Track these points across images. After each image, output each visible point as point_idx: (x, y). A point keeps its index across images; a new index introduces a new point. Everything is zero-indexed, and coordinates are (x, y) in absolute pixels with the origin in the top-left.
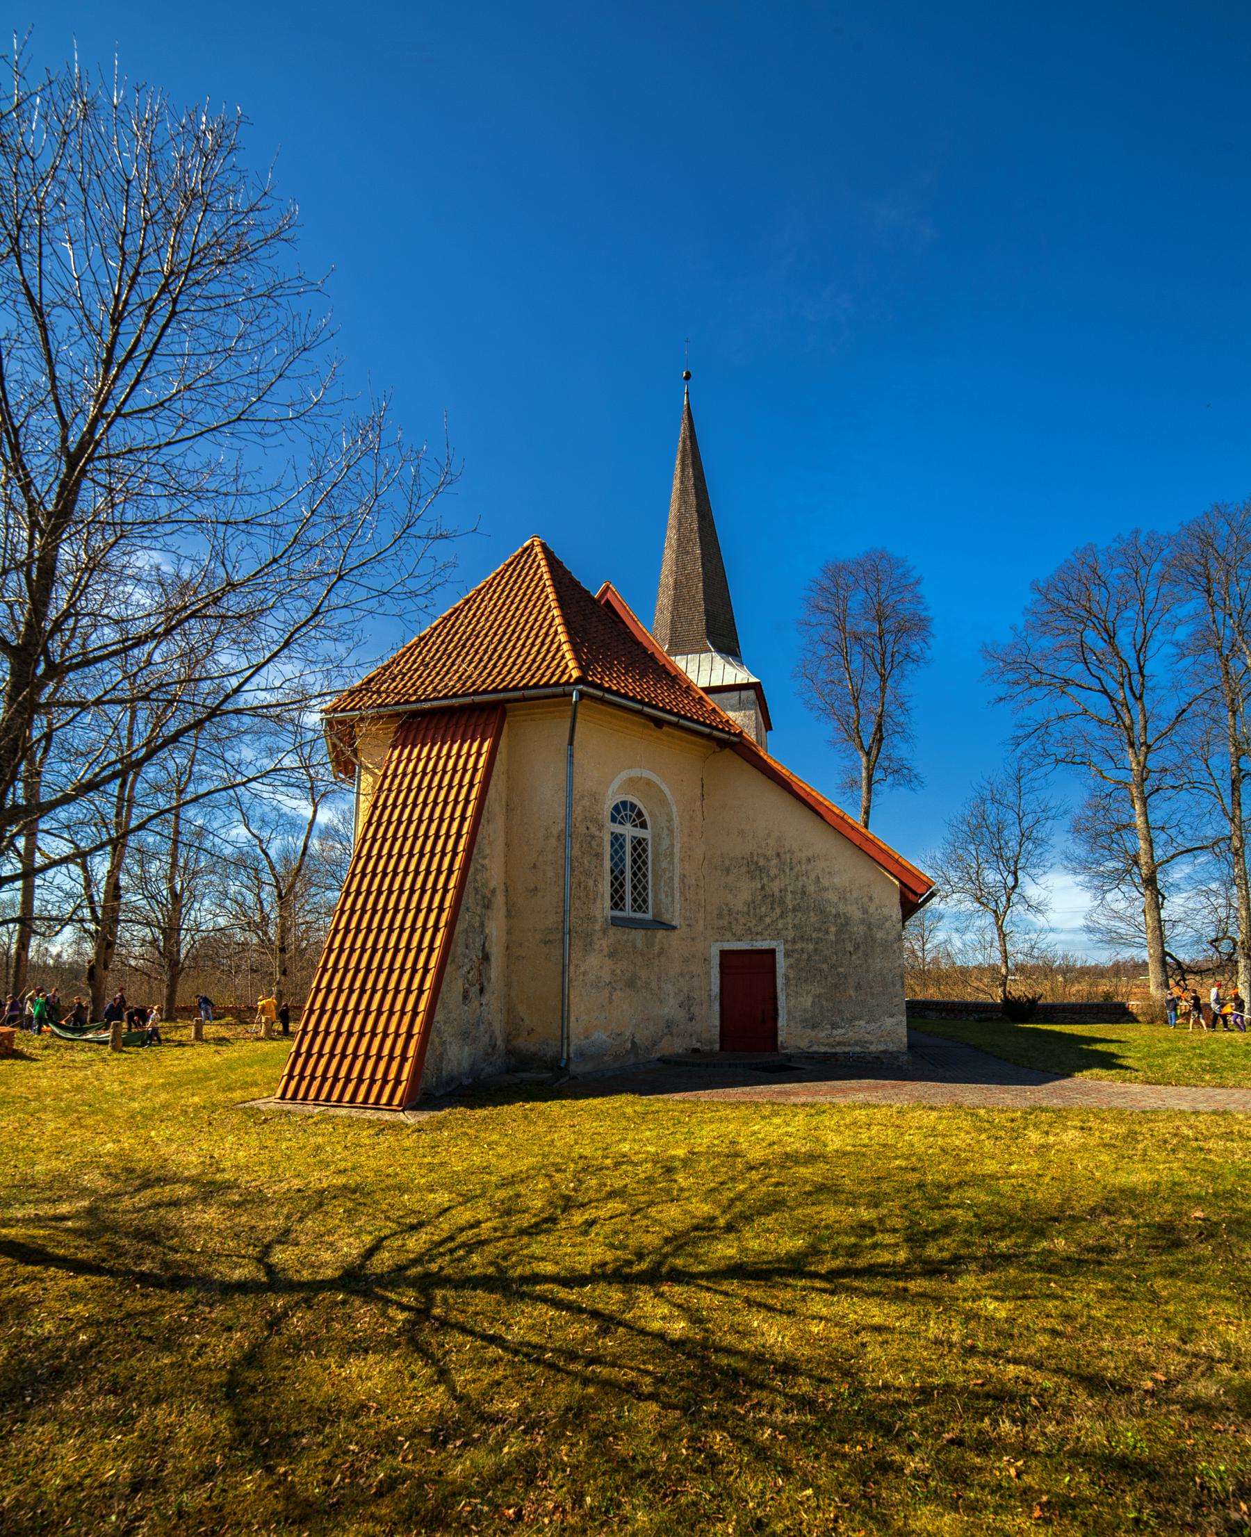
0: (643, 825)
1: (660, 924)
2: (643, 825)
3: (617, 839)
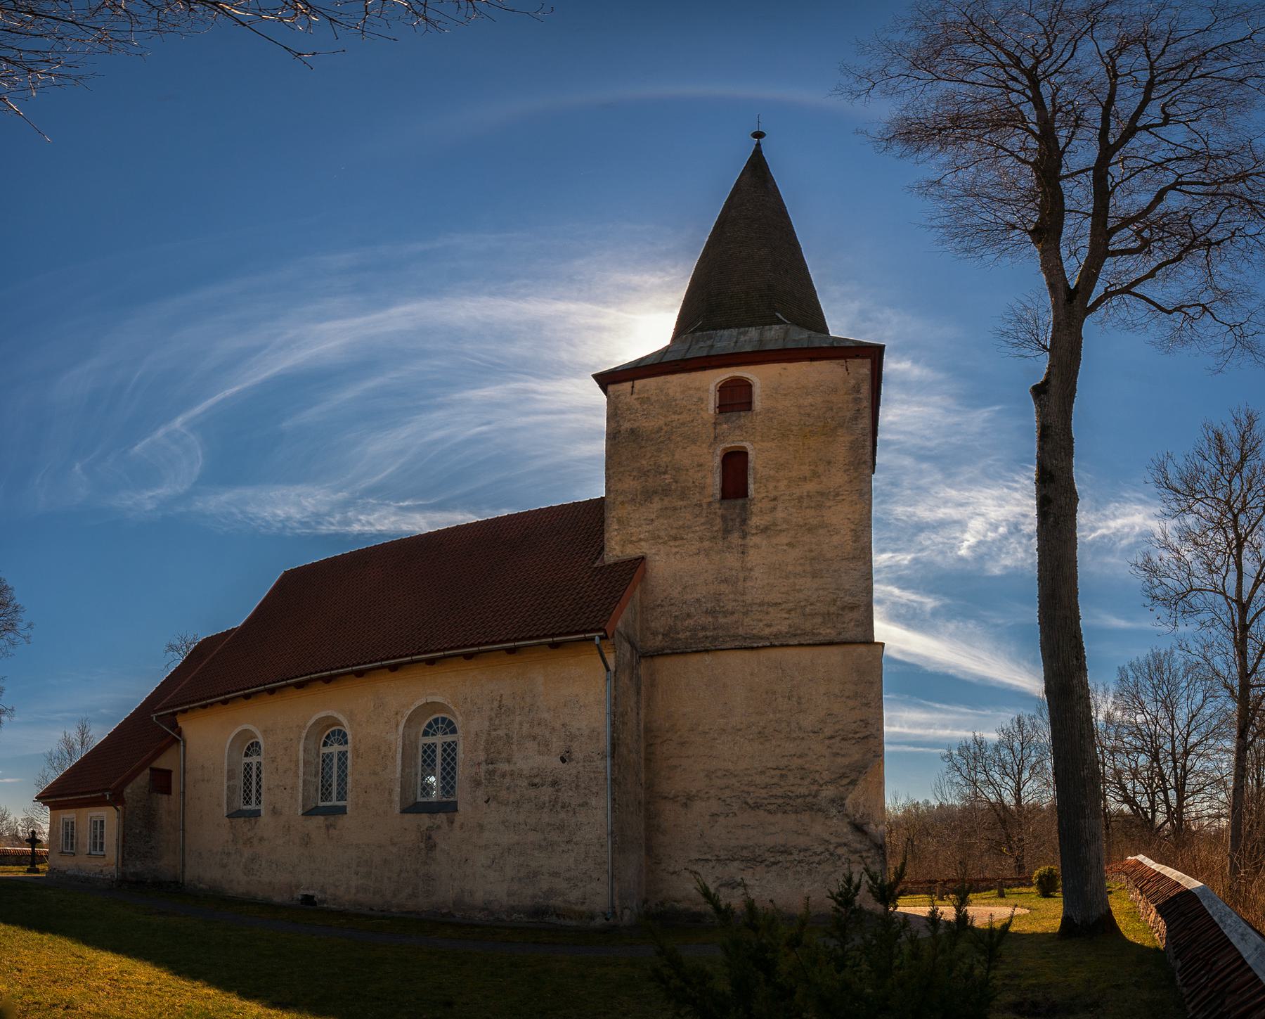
0: (454, 731)
2: (454, 731)
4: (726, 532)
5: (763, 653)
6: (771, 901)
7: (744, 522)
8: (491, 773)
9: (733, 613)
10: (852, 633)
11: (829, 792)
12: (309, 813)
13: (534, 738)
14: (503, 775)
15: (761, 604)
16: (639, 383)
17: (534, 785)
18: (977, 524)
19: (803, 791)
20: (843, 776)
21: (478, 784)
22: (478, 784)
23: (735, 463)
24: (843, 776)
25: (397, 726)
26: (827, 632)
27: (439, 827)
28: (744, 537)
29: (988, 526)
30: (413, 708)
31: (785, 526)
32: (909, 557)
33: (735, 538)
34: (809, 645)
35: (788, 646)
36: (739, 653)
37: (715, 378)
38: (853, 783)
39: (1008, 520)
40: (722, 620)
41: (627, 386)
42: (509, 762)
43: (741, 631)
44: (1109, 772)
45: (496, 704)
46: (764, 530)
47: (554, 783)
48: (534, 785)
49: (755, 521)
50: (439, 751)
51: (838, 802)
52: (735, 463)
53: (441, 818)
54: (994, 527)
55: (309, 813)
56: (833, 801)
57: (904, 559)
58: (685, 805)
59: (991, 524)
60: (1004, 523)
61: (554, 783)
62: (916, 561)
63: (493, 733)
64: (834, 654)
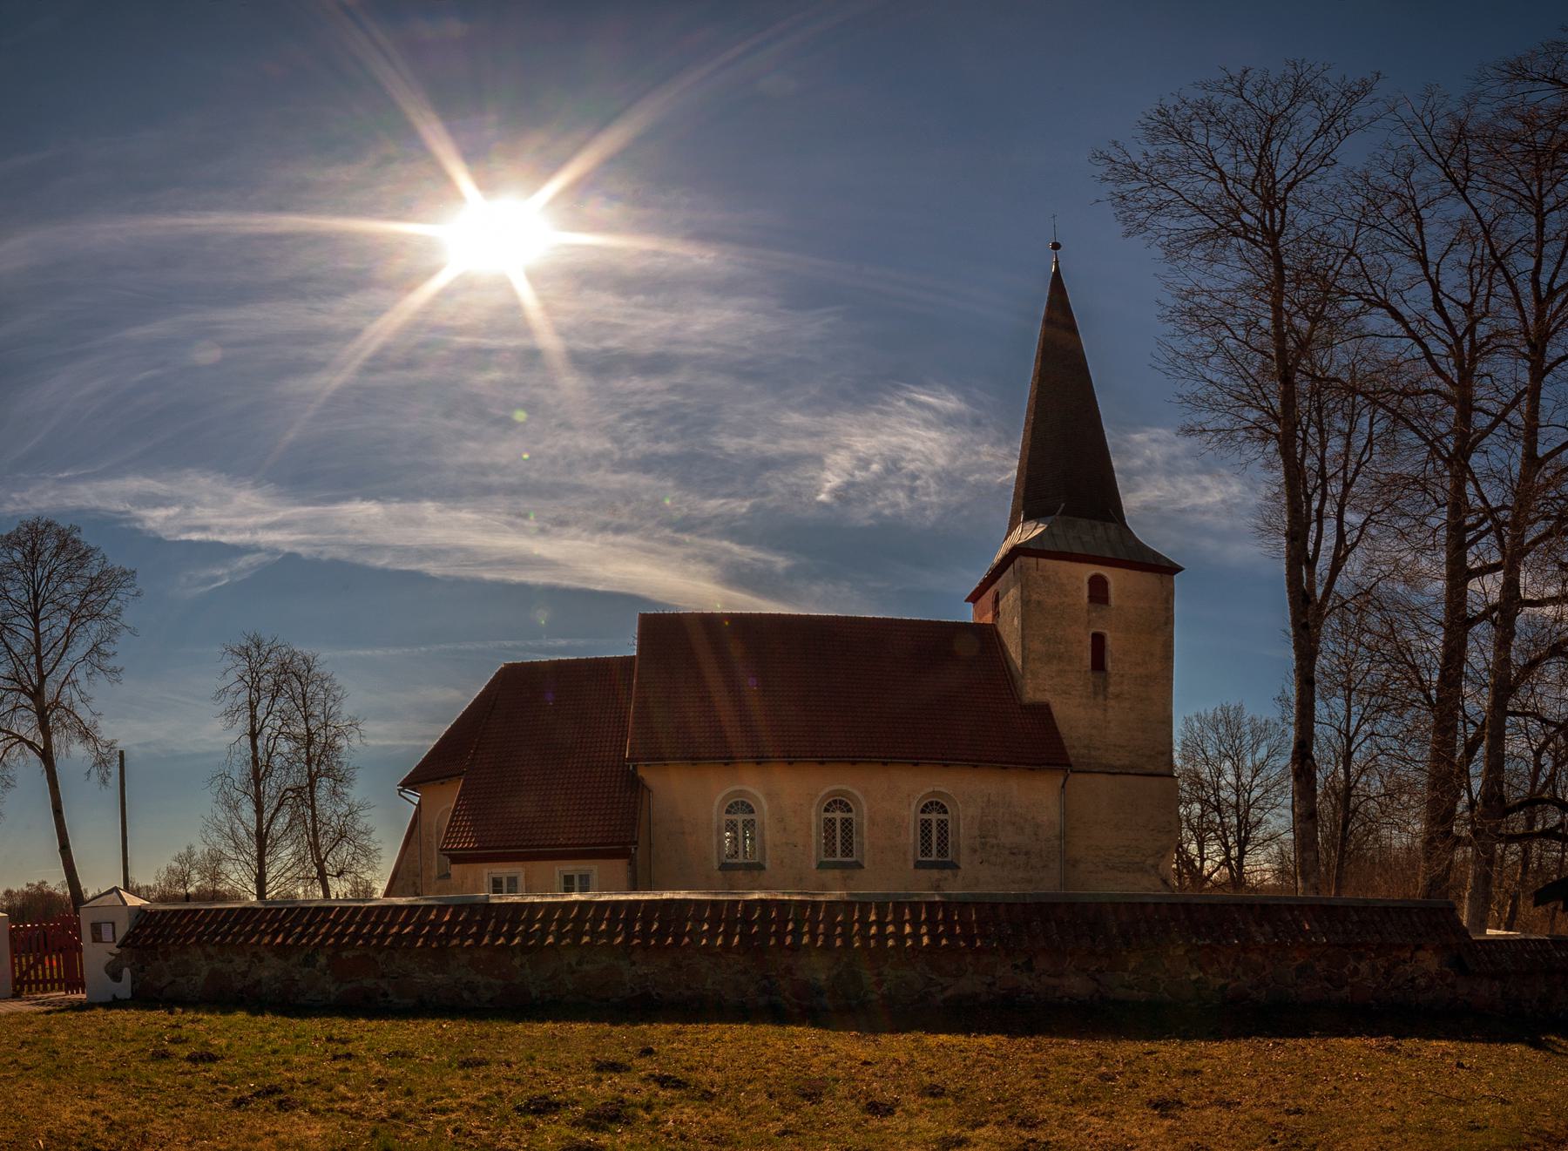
1: (859, 866)
3: (926, 825)
4: (1096, 694)
5: (1118, 777)
6: (111, 954)
7: (1105, 688)
8: (984, 844)
9: (1099, 749)
10: (1163, 770)
11: (1150, 861)
12: (822, 866)
13: (1014, 824)
14: (992, 847)
15: (1115, 745)
16: (1042, 561)
17: (1013, 854)
18: (842, 459)
19: (1137, 860)
20: (1158, 853)
21: (975, 851)
22: (975, 851)
23: (1098, 641)
24: (1158, 853)
25: (910, 805)
26: (1150, 768)
27: (946, 879)
28: (1105, 700)
29: (855, 462)
30: (923, 793)
31: (1127, 696)
32: (747, 504)
33: (1100, 698)
34: (1136, 774)
35: (1129, 774)
36: (1105, 776)
37: (1090, 570)
38: (1163, 856)
39: (881, 454)
40: (1093, 753)
41: (1032, 561)
42: (996, 838)
43: (1104, 761)
44: (200, 1016)
45: (985, 799)
46: (1117, 696)
47: (1027, 853)
48: (1013, 854)
49: (1111, 689)
50: (838, 825)
51: (1155, 867)
52: (1098, 641)
53: (948, 873)
54: (864, 463)
55: (822, 866)
56: (1153, 866)
57: (741, 507)
58: (1074, 866)
59: (860, 459)
60: (877, 458)
61: (1027, 853)
62: (755, 509)
63: (985, 818)
64: (1155, 781)
